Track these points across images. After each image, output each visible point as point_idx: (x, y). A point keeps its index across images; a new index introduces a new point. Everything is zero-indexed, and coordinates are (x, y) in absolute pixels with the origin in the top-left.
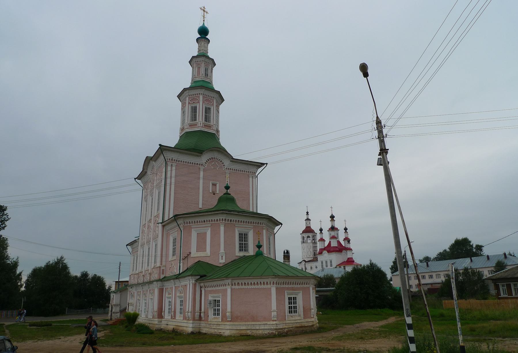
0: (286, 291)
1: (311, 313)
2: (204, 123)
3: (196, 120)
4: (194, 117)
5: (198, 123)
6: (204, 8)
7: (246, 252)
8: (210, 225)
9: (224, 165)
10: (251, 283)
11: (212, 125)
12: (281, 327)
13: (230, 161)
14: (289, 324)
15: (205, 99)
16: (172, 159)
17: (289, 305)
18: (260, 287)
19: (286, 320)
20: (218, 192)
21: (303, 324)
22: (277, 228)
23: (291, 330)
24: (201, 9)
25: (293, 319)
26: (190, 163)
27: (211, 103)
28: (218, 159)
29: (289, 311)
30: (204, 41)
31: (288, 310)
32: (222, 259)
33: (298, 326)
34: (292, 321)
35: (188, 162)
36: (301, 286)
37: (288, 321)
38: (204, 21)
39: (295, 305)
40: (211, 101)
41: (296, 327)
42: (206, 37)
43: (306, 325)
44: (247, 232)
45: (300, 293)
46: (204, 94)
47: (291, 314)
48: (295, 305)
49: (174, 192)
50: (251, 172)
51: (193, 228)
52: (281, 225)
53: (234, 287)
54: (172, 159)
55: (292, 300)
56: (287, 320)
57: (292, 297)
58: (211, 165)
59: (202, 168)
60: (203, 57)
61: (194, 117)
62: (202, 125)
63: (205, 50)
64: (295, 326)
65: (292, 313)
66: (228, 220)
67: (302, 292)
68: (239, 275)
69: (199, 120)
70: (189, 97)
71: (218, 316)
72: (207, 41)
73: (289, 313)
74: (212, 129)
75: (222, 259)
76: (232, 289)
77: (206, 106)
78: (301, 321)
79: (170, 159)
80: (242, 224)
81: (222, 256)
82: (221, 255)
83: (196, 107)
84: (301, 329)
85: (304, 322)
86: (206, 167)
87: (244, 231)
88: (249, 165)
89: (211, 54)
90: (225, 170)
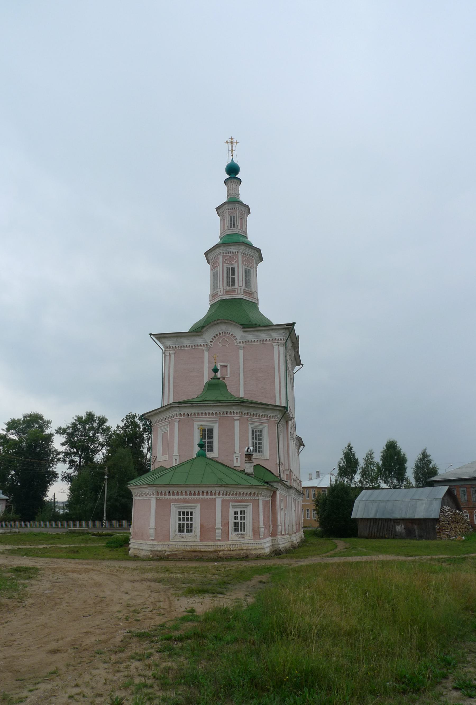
0: (231, 503)
1: (216, 535)
2: (225, 289)
3: (234, 285)
4: (231, 282)
5: (238, 289)
6: (232, 139)
7: (210, 452)
8: (167, 423)
9: (237, 339)
10: (207, 493)
11: (236, 289)
12: (159, 549)
13: (242, 331)
14: (176, 546)
15: (226, 258)
16: (170, 347)
17: (244, 521)
18: (206, 498)
19: (170, 541)
20: (229, 376)
21: (198, 548)
22: (297, 368)
23: (176, 554)
24: (227, 142)
25: (183, 540)
26: (192, 346)
27: (251, 264)
28: (227, 333)
29: (235, 529)
30: (231, 182)
31: (233, 527)
32: (237, 461)
33: (189, 549)
34: (178, 542)
35: (189, 346)
36: (201, 497)
37: (171, 542)
38: (232, 156)
39: (242, 521)
40: (251, 262)
41: (186, 551)
42: (236, 176)
43: (203, 550)
44: (211, 427)
45: (250, 506)
46: (225, 252)
47: (181, 534)
48: (242, 521)
49: (174, 385)
50: (275, 339)
51: (159, 427)
52: (301, 366)
53: (160, 497)
54: (170, 347)
55: (241, 515)
56: (171, 541)
57: (184, 512)
58: (218, 343)
59: (206, 349)
60: (226, 204)
61: (231, 282)
62: (222, 293)
63: (232, 194)
64: (182, 549)
65: (238, 531)
66: (184, 414)
67: (200, 505)
68: (273, 482)
69: (238, 285)
70: (223, 256)
71: (242, 533)
72: (239, 182)
73: (235, 531)
74: (237, 293)
75: (237, 461)
76: (223, 500)
77: (227, 267)
78: (195, 544)
79: (167, 347)
80: (204, 416)
81: (237, 459)
82: (235, 457)
83: (234, 269)
84: (194, 554)
85: (201, 545)
86: (212, 346)
87: (207, 425)
88: (271, 331)
89: (243, 198)
90: (239, 344)
